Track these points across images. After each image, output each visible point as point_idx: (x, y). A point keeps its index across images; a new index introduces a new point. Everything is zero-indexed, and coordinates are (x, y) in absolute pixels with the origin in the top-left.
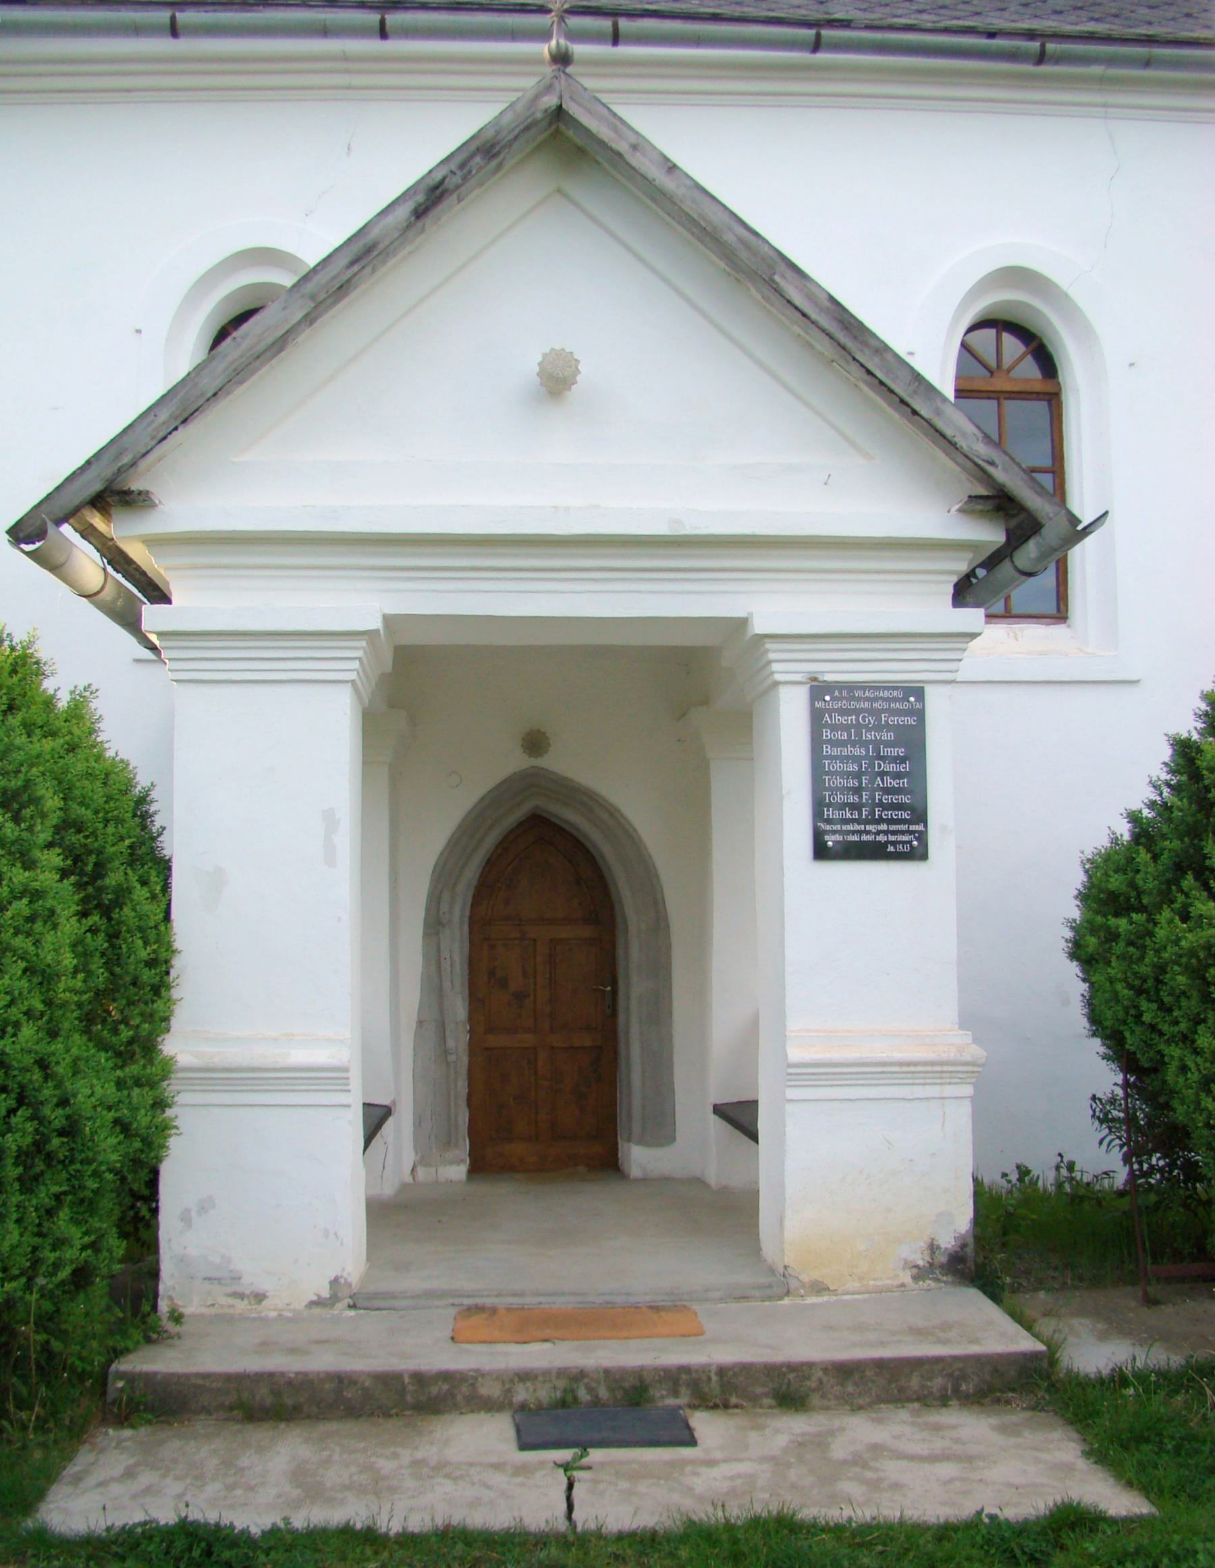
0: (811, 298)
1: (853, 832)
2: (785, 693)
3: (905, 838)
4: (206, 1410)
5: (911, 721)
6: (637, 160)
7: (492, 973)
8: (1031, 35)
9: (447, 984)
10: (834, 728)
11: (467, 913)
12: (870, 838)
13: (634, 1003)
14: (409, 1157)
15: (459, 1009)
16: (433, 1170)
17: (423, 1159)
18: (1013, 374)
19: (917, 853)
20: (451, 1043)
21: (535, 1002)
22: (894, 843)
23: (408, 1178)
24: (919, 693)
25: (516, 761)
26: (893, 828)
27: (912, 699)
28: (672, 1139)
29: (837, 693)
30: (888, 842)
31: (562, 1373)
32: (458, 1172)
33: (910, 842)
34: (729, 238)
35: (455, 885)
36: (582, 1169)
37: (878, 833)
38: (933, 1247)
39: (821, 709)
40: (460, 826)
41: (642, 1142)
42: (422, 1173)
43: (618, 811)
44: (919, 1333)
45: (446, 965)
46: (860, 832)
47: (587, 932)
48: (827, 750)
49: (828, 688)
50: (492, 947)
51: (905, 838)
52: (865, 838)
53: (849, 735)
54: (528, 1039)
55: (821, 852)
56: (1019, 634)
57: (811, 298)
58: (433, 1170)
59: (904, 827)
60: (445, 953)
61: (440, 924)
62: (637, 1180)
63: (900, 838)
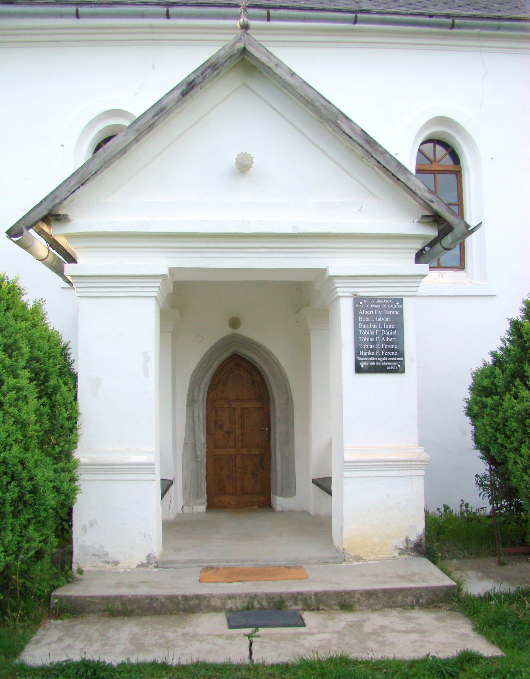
0: (353, 130)
1: (372, 361)
2: (342, 301)
3: (395, 364)
4: (93, 612)
5: (397, 313)
6: (277, 71)
7: (216, 423)
8: (448, 16)
9: (197, 427)
10: (364, 316)
11: (206, 397)
12: (380, 363)
13: (278, 435)
14: (180, 502)
15: (202, 438)
16: (191, 507)
17: (187, 503)
18: (441, 163)
19: (400, 370)
20: (199, 453)
21: (235, 435)
22: (390, 366)
23: (180, 511)
24: (401, 301)
25: (227, 331)
26: (389, 359)
27: (398, 303)
28: (294, 494)
29: (365, 301)
30: (387, 365)
31: (247, 595)
32: (202, 508)
33: (397, 365)
34: (318, 104)
35: (200, 384)
36: (255, 507)
37: (383, 361)
38: (407, 541)
39: (358, 308)
40: (202, 359)
41: (281, 495)
42: (186, 509)
43: (271, 352)
44: (401, 578)
45: (197, 419)
46: (375, 361)
47: (257, 404)
48: (361, 325)
49: (361, 299)
50: (216, 411)
51: (395, 364)
52: (377, 363)
53: (371, 319)
54: (232, 451)
55: (358, 370)
56: (444, 275)
57: (353, 130)
58: (191, 507)
59: (394, 359)
60: (196, 414)
61: (194, 401)
62: (279, 512)
63: (393, 363)
